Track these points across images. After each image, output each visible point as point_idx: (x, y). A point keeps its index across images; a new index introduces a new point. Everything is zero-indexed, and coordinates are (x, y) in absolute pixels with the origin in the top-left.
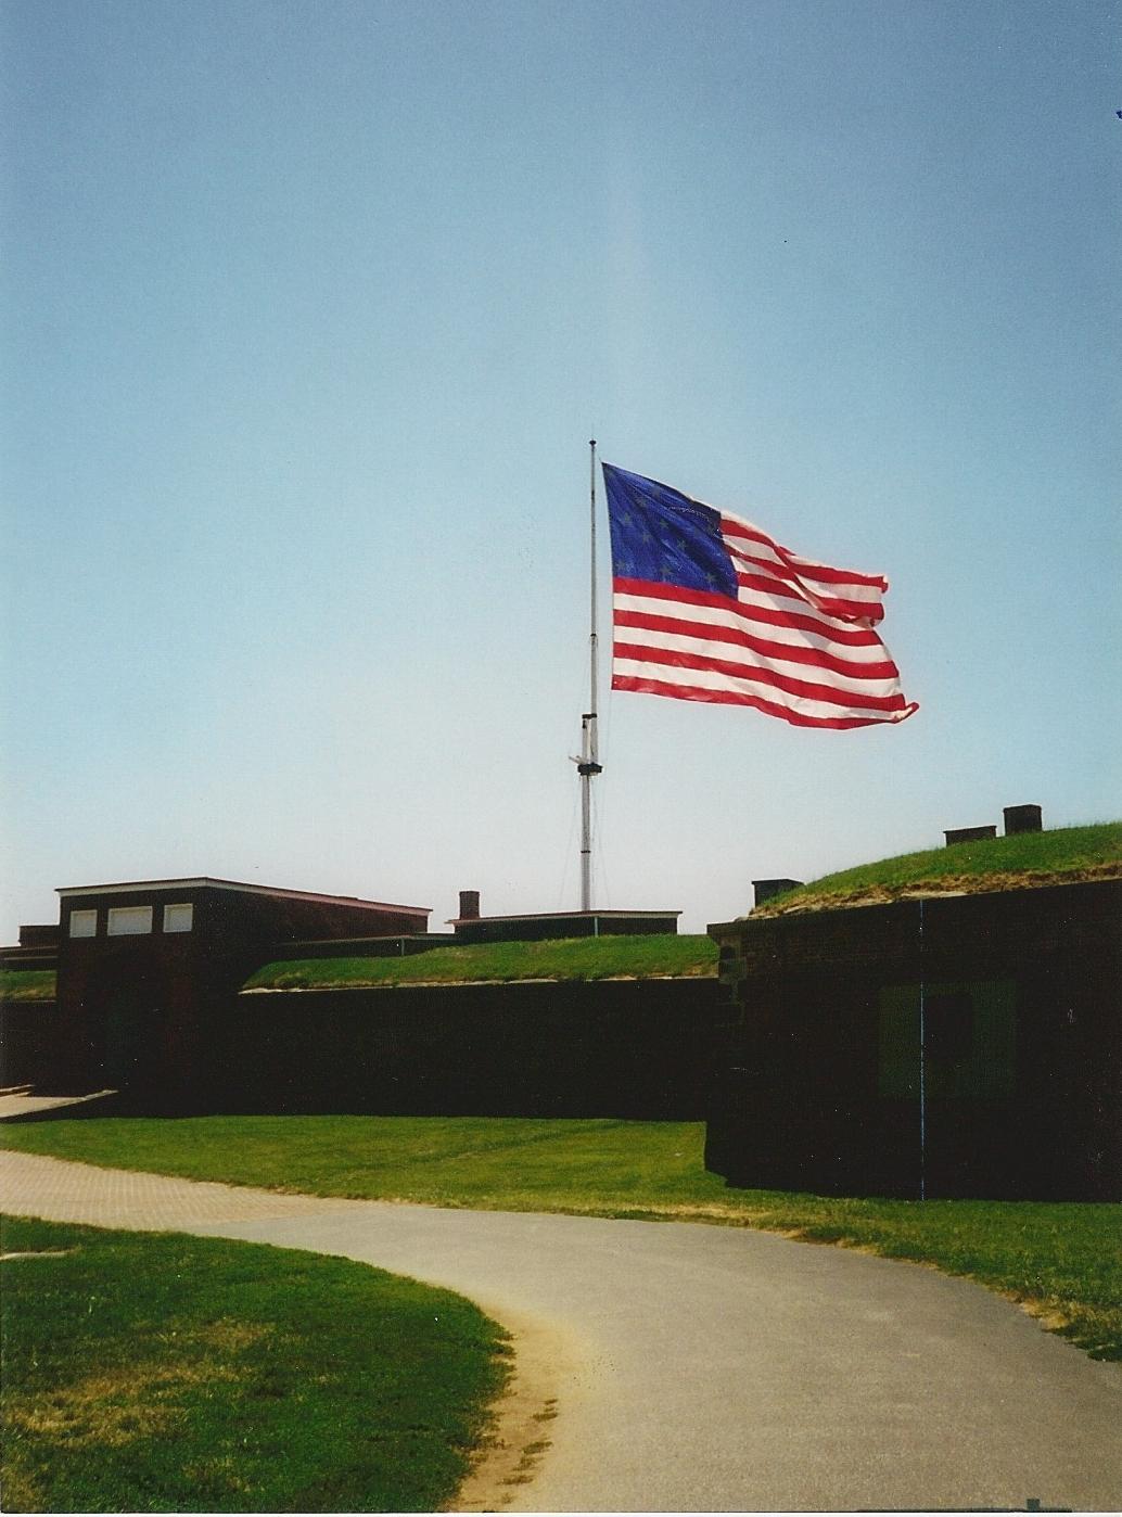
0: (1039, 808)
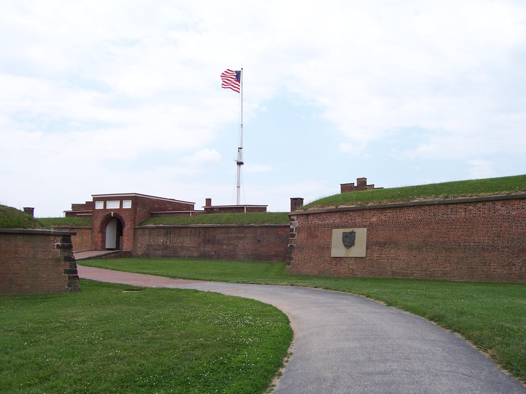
0: (211, 199)
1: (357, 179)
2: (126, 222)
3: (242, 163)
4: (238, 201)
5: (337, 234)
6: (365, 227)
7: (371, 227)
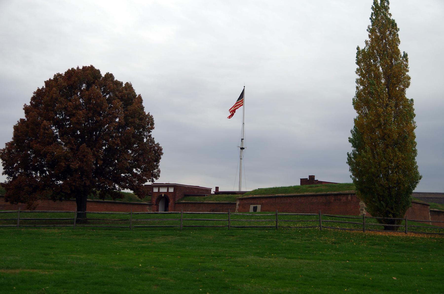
1: (309, 176)
2: (170, 200)
3: (244, 148)
4: (240, 187)
5: (252, 207)
6: (260, 204)
7: (262, 205)
